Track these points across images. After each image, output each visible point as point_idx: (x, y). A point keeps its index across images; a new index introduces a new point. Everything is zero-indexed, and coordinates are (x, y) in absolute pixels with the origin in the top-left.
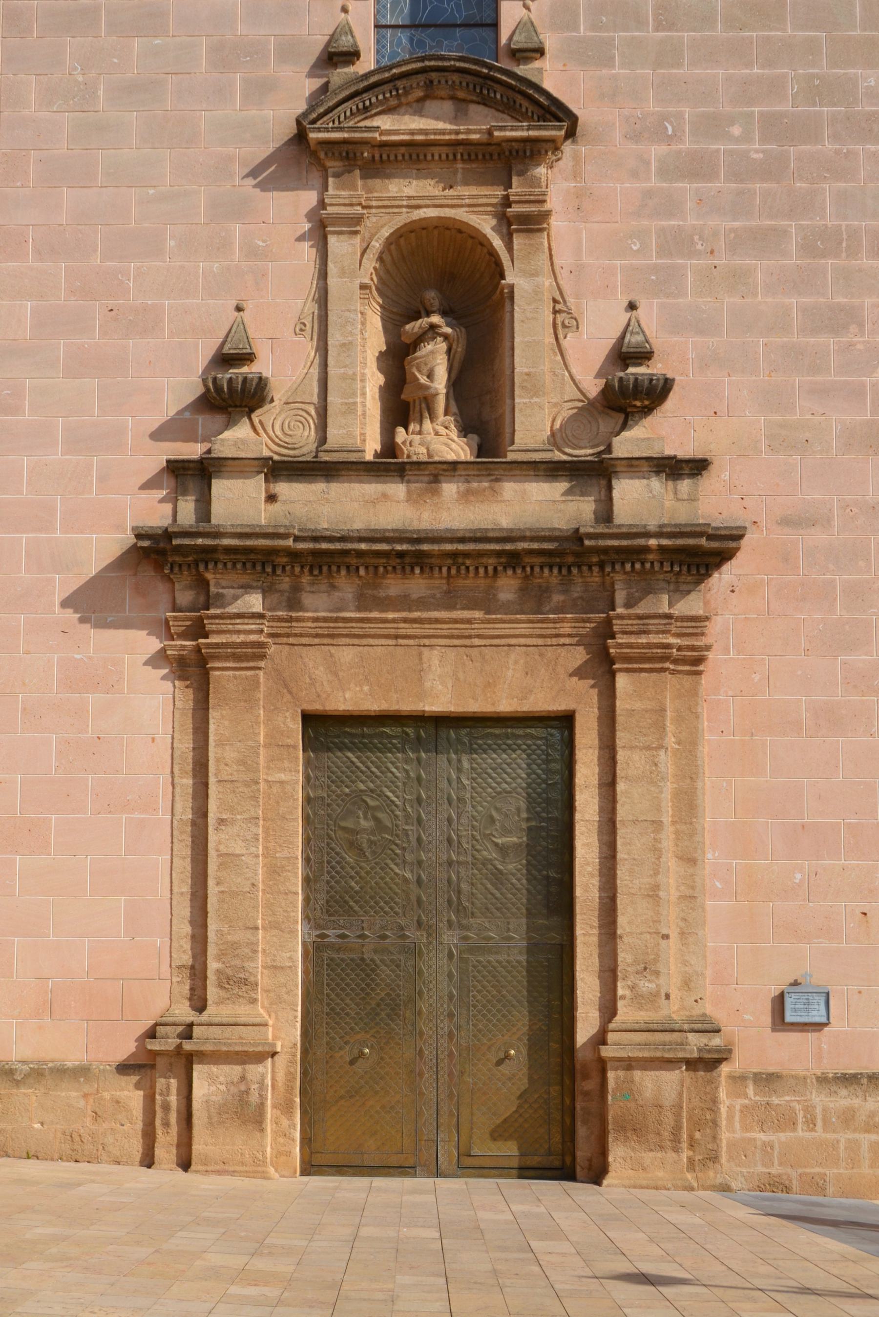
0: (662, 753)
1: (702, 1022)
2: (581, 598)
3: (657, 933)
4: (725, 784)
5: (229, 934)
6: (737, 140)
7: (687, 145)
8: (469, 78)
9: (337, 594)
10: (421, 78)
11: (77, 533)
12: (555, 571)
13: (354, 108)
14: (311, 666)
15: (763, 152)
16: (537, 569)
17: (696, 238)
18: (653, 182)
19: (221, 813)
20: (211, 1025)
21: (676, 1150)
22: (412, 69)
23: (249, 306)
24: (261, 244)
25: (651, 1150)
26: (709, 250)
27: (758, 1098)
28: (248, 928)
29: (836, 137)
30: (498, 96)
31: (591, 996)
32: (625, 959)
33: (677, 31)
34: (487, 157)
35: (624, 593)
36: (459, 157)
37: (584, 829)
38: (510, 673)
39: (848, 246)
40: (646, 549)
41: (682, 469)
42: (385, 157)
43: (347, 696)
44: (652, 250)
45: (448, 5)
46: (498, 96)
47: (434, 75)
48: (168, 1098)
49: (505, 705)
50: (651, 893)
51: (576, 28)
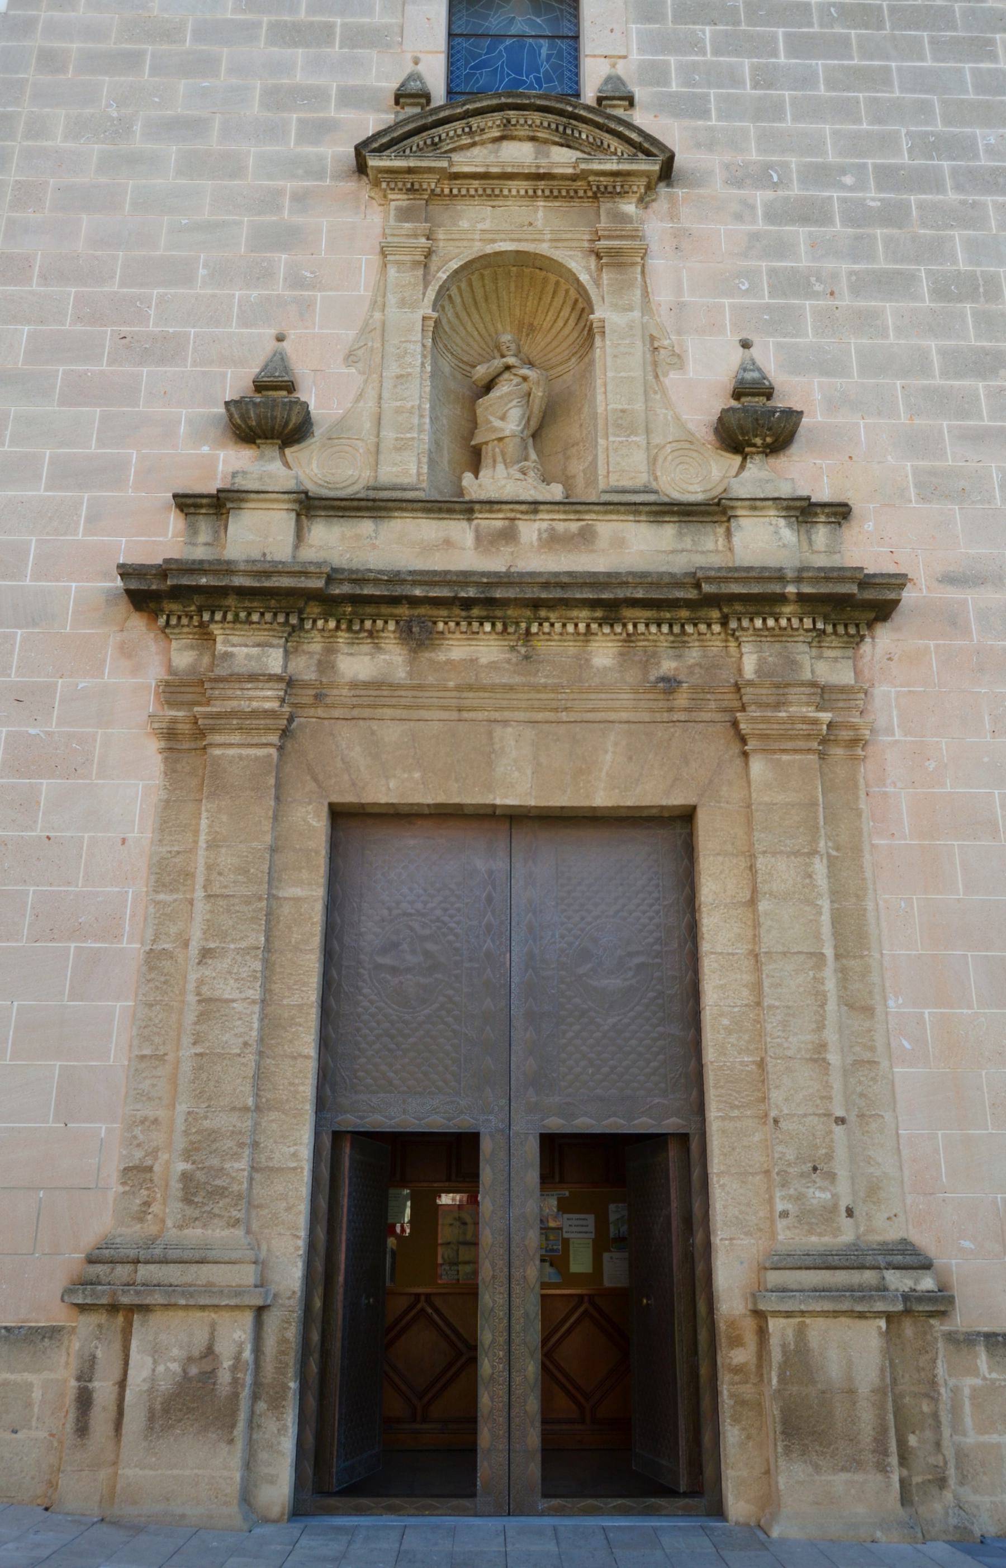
0: (817, 860)
1: (903, 1252)
2: (699, 665)
3: (828, 1115)
4: (903, 905)
5: (206, 1118)
6: (851, 189)
7: (796, 190)
8: (551, 117)
9: (383, 657)
10: (497, 117)
11: (51, 581)
12: (665, 629)
13: (421, 143)
14: (344, 746)
15: (880, 200)
16: (641, 628)
17: (813, 279)
18: (761, 225)
19: (207, 940)
20: (167, 1262)
21: (882, 1468)
22: (488, 106)
23: (292, 334)
24: (309, 275)
25: (843, 1469)
26: (829, 291)
27: (994, 1375)
28: (233, 1109)
29: (958, 188)
30: (584, 136)
31: (737, 1213)
32: (784, 1154)
33: (776, 89)
34: (572, 193)
35: (755, 656)
36: (539, 193)
37: (715, 965)
38: (609, 757)
39: (986, 292)
40: (782, 599)
41: (816, 514)
42: (455, 191)
43: (391, 785)
44: (763, 290)
45: (527, 77)
46: (584, 136)
47: (512, 113)
48: (90, 1385)
49: (602, 798)
50: (816, 1056)
51: (667, 83)
